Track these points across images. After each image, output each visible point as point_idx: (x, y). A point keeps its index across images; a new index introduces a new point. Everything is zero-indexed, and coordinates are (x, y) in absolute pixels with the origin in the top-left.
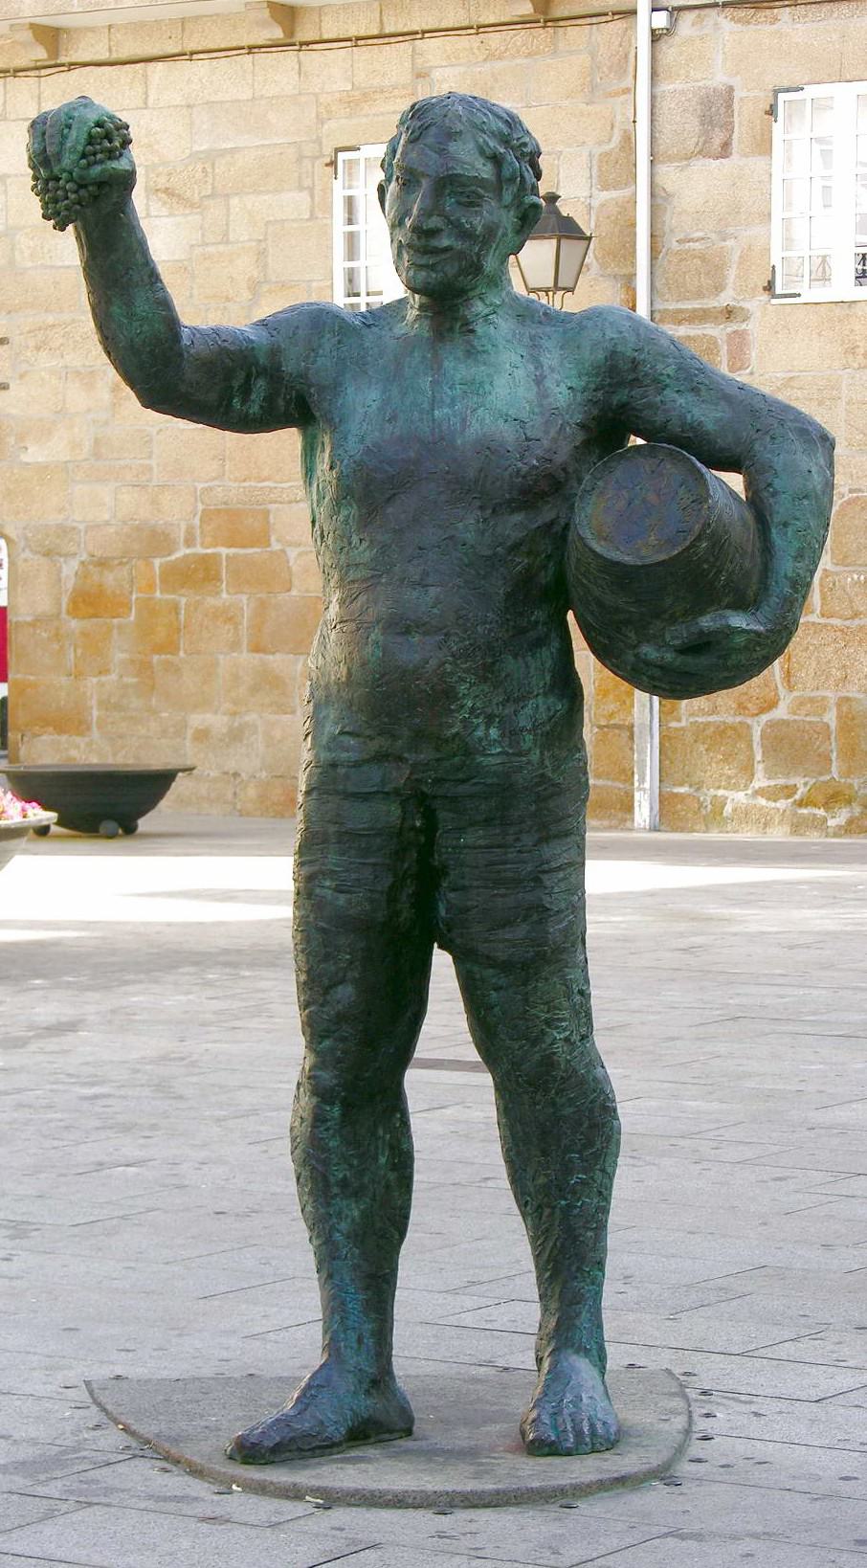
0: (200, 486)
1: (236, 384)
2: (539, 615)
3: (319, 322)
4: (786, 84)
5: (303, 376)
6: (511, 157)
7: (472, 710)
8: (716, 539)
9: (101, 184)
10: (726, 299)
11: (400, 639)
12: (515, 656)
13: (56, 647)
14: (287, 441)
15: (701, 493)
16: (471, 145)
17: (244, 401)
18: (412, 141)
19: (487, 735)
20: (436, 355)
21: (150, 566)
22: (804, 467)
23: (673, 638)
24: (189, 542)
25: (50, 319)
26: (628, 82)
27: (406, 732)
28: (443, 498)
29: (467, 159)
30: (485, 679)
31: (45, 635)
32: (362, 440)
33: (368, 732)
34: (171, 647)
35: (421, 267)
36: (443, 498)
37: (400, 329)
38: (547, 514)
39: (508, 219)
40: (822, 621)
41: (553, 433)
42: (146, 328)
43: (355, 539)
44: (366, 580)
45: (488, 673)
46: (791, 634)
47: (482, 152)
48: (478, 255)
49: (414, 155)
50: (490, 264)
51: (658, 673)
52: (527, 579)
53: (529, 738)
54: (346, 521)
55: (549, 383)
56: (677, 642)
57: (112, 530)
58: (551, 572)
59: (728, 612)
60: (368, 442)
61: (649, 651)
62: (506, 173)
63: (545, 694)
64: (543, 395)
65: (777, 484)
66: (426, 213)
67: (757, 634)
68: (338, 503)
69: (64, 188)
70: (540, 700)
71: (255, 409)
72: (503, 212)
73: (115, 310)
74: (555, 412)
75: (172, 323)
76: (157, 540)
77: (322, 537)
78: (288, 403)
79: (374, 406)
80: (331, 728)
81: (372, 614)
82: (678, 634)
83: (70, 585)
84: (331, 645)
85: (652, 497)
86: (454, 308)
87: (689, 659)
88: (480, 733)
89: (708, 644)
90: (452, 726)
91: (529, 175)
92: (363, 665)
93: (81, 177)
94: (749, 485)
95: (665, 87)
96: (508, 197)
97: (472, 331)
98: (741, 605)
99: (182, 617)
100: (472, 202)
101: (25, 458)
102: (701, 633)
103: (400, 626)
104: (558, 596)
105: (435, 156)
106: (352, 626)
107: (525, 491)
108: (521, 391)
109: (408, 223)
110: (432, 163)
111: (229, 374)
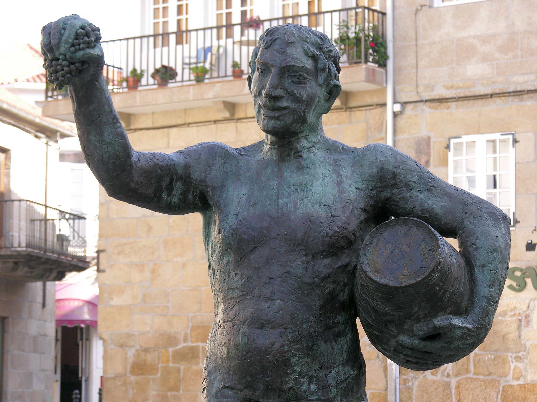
0: (190, 315)
1: (164, 185)
2: (340, 318)
3: (214, 152)
4: (454, 135)
5: (203, 181)
6: (322, 57)
7: (300, 374)
8: (442, 272)
9: (83, 63)
11: (257, 331)
12: (326, 342)
13: (124, 388)
14: (196, 219)
15: (435, 248)
16: (300, 50)
17: (169, 195)
18: (266, 48)
19: (309, 388)
20: (280, 169)
21: (167, 351)
22: (494, 234)
23: (419, 331)
24: (185, 340)
25: (124, 241)
26: (383, 135)
27: (261, 387)
29: (298, 57)
30: (308, 355)
31: (119, 383)
32: (237, 216)
33: (239, 387)
34: (176, 388)
35: (271, 118)
37: (259, 156)
38: (344, 260)
39: (321, 93)
40: (475, 377)
41: (348, 213)
42: (110, 149)
43: (232, 274)
44: (238, 297)
45: (310, 351)
46: (488, 330)
47: (306, 53)
48: (304, 112)
49: (267, 55)
50: (311, 118)
51: (409, 352)
52: (332, 297)
53: (334, 390)
54: (227, 264)
55: (345, 185)
56: (421, 333)
57: (150, 335)
58: (346, 294)
59: (451, 316)
60: (240, 218)
61: (404, 339)
62: (320, 66)
63: (343, 365)
64: (342, 191)
65: (478, 243)
66: (274, 87)
67: (468, 329)
68: (223, 254)
69: (61, 65)
70: (340, 368)
71: (175, 200)
72: (318, 88)
73: (92, 138)
74: (349, 201)
75: (126, 147)
76: (171, 340)
77: (214, 274)
78: (195, 197)
79: (244, 197)
80: (218, 385)
81: (241, 318)
82: (421, 329)
83: (131, 360)
84: (218, 336)
85: (405, 248)
86: (290, 143)
87: (428, 343)
88: (305, 387)
89: (439, 334)
90: (288, 383)
91: (333, 69)
92: (237, 346)
93: (71, 58)
94: (461, 245)
95: (400, 137)
96: (321, 79)
97: (301, 156)
98: (459, 312)
99: (182, 374)
100: (301, 82)
101: (112, 303)
102: (435, 327)
103: (259, 323)
104: (351, 309)
105: (279, 55)
106: (230, 324)
107: (331, 246)
108: (329, 189)
109: (264, 93)
110: (277, 59)
111: (160, 179)
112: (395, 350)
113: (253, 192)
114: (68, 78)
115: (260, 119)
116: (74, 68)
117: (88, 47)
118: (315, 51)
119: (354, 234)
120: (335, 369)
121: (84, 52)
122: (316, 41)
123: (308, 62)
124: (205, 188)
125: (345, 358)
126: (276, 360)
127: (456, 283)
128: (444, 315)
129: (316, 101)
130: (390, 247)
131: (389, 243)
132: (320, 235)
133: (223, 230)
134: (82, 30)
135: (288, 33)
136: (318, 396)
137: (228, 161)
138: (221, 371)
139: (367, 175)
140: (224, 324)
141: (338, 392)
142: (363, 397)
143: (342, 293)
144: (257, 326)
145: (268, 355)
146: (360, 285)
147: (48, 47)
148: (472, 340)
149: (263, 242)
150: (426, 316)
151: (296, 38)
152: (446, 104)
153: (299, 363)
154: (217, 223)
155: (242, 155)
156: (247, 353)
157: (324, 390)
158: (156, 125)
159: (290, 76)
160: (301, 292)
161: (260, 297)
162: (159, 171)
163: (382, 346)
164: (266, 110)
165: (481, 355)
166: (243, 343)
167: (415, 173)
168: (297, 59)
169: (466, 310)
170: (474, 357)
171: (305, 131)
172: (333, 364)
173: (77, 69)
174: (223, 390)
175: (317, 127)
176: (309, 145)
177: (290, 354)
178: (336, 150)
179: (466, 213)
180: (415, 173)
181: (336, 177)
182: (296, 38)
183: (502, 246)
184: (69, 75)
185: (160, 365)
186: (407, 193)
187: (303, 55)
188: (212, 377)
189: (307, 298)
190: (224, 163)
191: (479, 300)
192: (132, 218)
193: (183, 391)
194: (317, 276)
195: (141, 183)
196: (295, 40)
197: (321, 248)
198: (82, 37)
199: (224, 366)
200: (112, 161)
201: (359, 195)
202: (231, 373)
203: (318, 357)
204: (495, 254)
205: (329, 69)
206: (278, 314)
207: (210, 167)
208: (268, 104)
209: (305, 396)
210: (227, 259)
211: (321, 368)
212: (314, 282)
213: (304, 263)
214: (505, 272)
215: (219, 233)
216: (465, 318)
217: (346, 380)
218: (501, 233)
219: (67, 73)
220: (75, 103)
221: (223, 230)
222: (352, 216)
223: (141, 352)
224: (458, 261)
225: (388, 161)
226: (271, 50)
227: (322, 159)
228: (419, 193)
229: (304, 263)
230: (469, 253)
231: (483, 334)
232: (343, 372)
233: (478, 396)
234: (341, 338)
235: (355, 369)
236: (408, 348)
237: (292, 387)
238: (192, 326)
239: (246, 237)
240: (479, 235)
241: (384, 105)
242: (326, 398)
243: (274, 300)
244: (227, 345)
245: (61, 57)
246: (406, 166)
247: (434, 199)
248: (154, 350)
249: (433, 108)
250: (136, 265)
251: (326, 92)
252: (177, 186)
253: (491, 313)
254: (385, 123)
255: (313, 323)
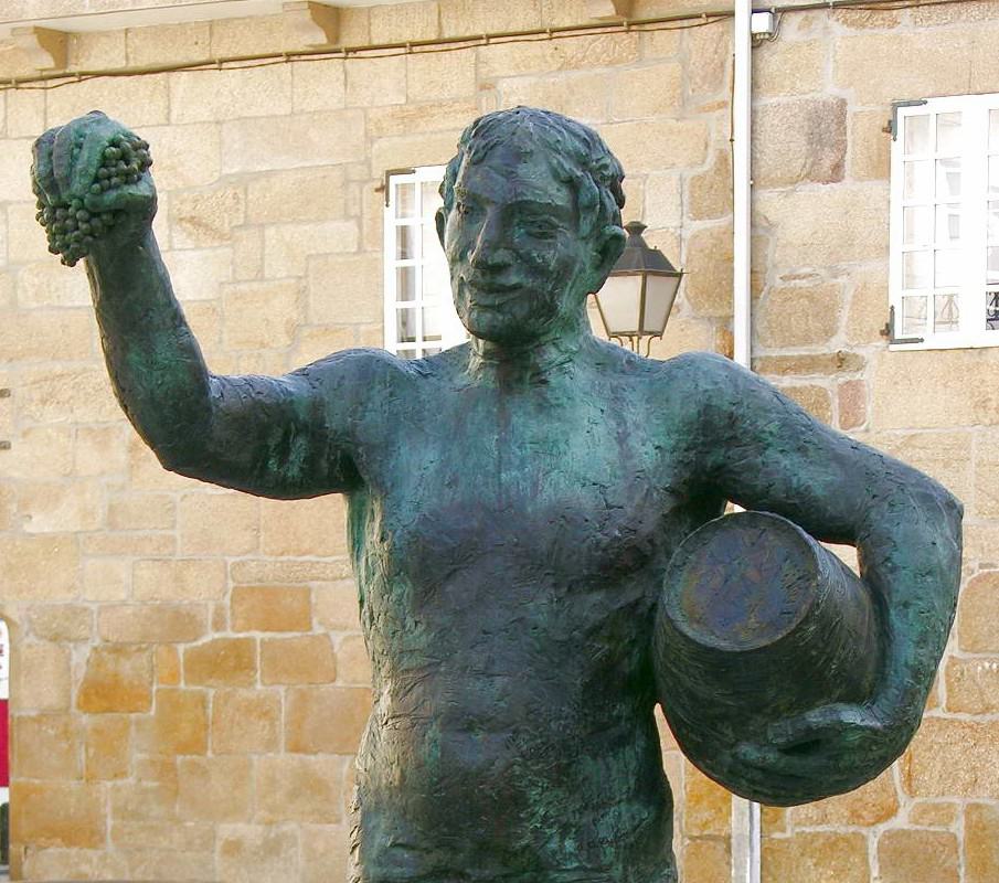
0: (231, 560)
1: (272, 443)
2: (622, 709)
3: (368, 371)
4: (907, 97)
5: (350, 433)
6: (589, 181)
7: (545, 818)
8: (826, 622)
9: (116, 212)
10: (837, 344)
11: (461, 737)
12: (594, 757)
13: (65, 745)
14: (331, 509)
15: (808, 569)
16: (543, 168)
18: (475, 163)
19: (562, 847)
20: (502, 409)
21: (173, 652)
22: (928, 538)
24: (218, 624)
25: (58, 368)
26: (725, 94)
27: (468, 844)
28: (511, 574)
29: (539, 183)
30: (560, 784)
31: (52, 732)
32: (418, 507)
33: (424, 844)
34: (197, 746)
35: (486, 308)
36: (511, 574)
37: (462, 379)
38: (631, 593)
39: (586, 253)
40: (948, 716)
41: (638, 499)
42: (168, 378)
43: (410, 622)
44: (422, 669)
45: (563, 776)
46: (912, 731)
47: (556, 176)
48: (552, 294)
49: (477, 179)
50: (565, 304)
51: (759, 776)
52: (608, 667)
53: (610, 850)
54: (399, 601)
55: (634, 442)
56: (781, 741)
57: (129, 611)
58: (635, 659)
59: (840, 706)
60: (425, 510)
61: (748, 751)
62: (584, 199)
63: (629, 801)
64: (626, 455)
65: (897, 558)
66: (491, 246)
67: (874, 730)
68: (390, 580)
69: (73, 217)
70: (623, 807)
71: (294, 472)
72: (580, 244)
73: (133, 357)
74: (640, 475)
75: (199, 372)
76: (181, 623)
77: (372, 619)
78: (332, 465)
79: (432, 468)
80: (382, 840)
81: (429, 708)
82: (782, 730)
83: (81, 674)
84: (382, 743)
85: (752, 573)
86: (524, 356)
87: (795, 760)
88: (553, 845)
89: (817, 742)
90: (521, 837)
91: (610, 202)
92: (419, 766)
93: (94, 205)
94: (864, 560)
95: (767, 100)
96: (585, 227)
97: (545, 382)
98: (855, 697)
99: (210, 712)
100: (544, 233)
101: (29, 528)
102: (809, 730)
103: (462, 721)
104: (644, 688)
105: (501, 180)
106: (406, 722)
107: (605, 566)
108: (601, 451)
109: (471, 257)
110: (499, 188)
111: (264, 432)
112: (730, 772)
113: (450, 456)
114: (88, 244)
115: (463, 308)
116: (100, 225)
117: (126, 183)
118: (575, 169)
119: (651, 541)
120: (613, 809)
121: (119, 192)
122: (575, 148)
123: (559, 194)
124: (353, 448)
125: (633, 787)
126: (498, 793)
127: (850, 640)
128: (827, 703)
129: (576, 269)
130: (723, 573)
131: (721, 562)
132: (585, 546)
133: (390, 534)
134: (114, 149)
135: (519, 132)
136: (580, 861)
137: (398, 391)
138: (388, 814)
139: (677, 421)
140: (394, 721)
141: (617, 854)
142: (669, 860)
143: (626, 660)
144: (460, 727)
145: (482, 783)
146: (663, 646)
147: (47, 182)
148: (881, 752)
149: (471, 559)
150: (791, 707)
151: (535, 143)
152: (886, 14)
153: (542, 802)
154: (378, 520)
155: (426, 376)
156: (441, 779)
157: (592, 851)
158: (132, 65)
159: (522, 223)
160: (545, 659)
161: (464, 669)
162: (262, 416)
163: (704, 762)
164: (475, 291)
165: (965, 662)
166: (432, 759)
167: (774, 415)
168: (537, 188)
169: (871, 693)
170: (947, 667)
171: (554, 332)
172: (610, 799)
173: (104, 225)
174: (394, 851)
175: (577, 320)
176: (561, 359)
177: (524, 783)
178: (615, 365)
179: (874, 496)
180: (774, 415)
181: (615, 426)
182: (535, 143)
183: (945, 561)
184: (90, 239)
185: (155, 688)
186: (756, 457)
187: (550, 179)
188: (371, 825)
189: (557, 671)
190: (391, 394)
191: (896, 671)
192: (79, 308)
193: (214, 752)
194: (577, 628)
195: (228, 442)
196: (533, 147)
197: (585, 572)
198: (114, 162)
199: (394, 804)
200: (171, 403)
201: (662, 461)
202: (408, 817)
203: (578, 787)
204: (929, 579)
205: (602, 203)
206: (502, 704)
207: (361, 404)
208: (480, 279)
209: (555, 863)
210: (399, 591)
211: (586, 808)
212: (571, 639)
213: (552, 601)
214: (948, 614)
215: (382, 540)
216: (868, 707)
217: (634, 829)
218: (942, 535)
219: (85, 235)
220: (98, 286)
221: (390, 534)
222: (647, 504)
223: (105, 654)
224: (856, 598)
225: (720, 389)
226: (484, 168)
227: (588, 389)
228: (780, 456)
229: (552, 601)
230: (879, 577)
231: (904, 738)
232: (629, 815)
233: (956, 763)
234: (624, 747)
235: (651, 808)
236: (756, 768)
237: (528, 846)
238: (235, 589)
239: (436, 549)
240: (898, 541)
241: (731, 14)
242: (596, 866)
243: (493, 675)
244: (401, 762)
245: (74, 202)
246: (756, 401)
247: (811, 468)
248: (139, 650)
249: (852, 24)
250: (90, 430)
251: (596, 251)
252: (298, 445)
253: (919, 697)
254: (729, 64)
255: (569, 721)
